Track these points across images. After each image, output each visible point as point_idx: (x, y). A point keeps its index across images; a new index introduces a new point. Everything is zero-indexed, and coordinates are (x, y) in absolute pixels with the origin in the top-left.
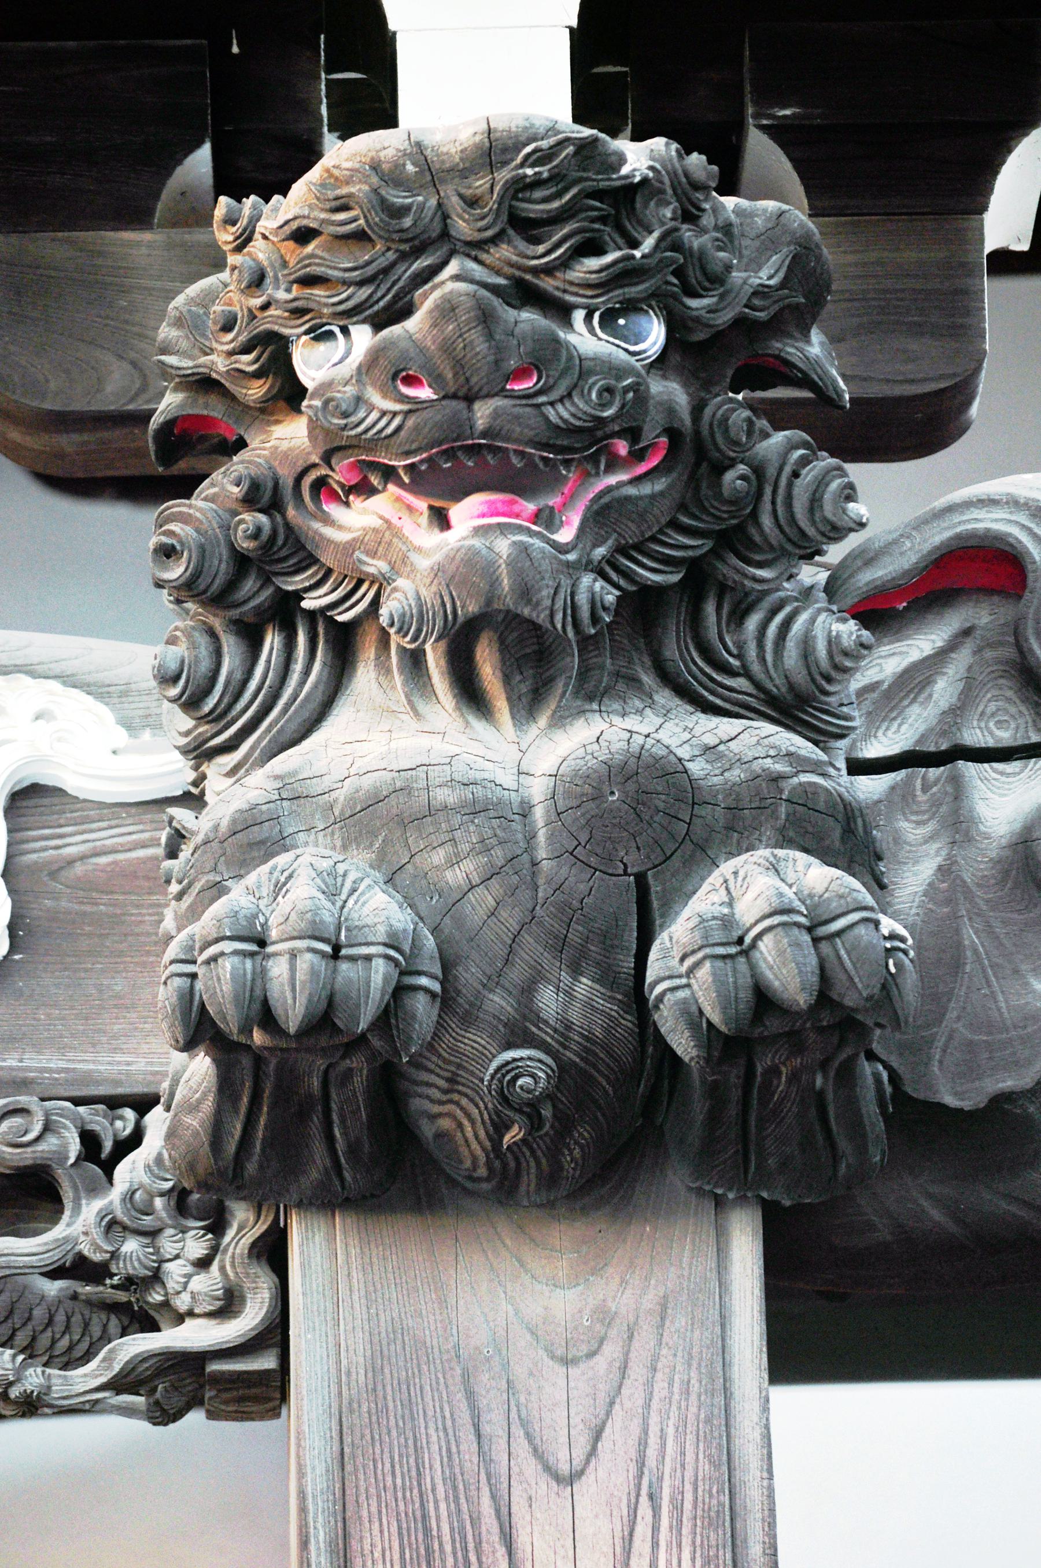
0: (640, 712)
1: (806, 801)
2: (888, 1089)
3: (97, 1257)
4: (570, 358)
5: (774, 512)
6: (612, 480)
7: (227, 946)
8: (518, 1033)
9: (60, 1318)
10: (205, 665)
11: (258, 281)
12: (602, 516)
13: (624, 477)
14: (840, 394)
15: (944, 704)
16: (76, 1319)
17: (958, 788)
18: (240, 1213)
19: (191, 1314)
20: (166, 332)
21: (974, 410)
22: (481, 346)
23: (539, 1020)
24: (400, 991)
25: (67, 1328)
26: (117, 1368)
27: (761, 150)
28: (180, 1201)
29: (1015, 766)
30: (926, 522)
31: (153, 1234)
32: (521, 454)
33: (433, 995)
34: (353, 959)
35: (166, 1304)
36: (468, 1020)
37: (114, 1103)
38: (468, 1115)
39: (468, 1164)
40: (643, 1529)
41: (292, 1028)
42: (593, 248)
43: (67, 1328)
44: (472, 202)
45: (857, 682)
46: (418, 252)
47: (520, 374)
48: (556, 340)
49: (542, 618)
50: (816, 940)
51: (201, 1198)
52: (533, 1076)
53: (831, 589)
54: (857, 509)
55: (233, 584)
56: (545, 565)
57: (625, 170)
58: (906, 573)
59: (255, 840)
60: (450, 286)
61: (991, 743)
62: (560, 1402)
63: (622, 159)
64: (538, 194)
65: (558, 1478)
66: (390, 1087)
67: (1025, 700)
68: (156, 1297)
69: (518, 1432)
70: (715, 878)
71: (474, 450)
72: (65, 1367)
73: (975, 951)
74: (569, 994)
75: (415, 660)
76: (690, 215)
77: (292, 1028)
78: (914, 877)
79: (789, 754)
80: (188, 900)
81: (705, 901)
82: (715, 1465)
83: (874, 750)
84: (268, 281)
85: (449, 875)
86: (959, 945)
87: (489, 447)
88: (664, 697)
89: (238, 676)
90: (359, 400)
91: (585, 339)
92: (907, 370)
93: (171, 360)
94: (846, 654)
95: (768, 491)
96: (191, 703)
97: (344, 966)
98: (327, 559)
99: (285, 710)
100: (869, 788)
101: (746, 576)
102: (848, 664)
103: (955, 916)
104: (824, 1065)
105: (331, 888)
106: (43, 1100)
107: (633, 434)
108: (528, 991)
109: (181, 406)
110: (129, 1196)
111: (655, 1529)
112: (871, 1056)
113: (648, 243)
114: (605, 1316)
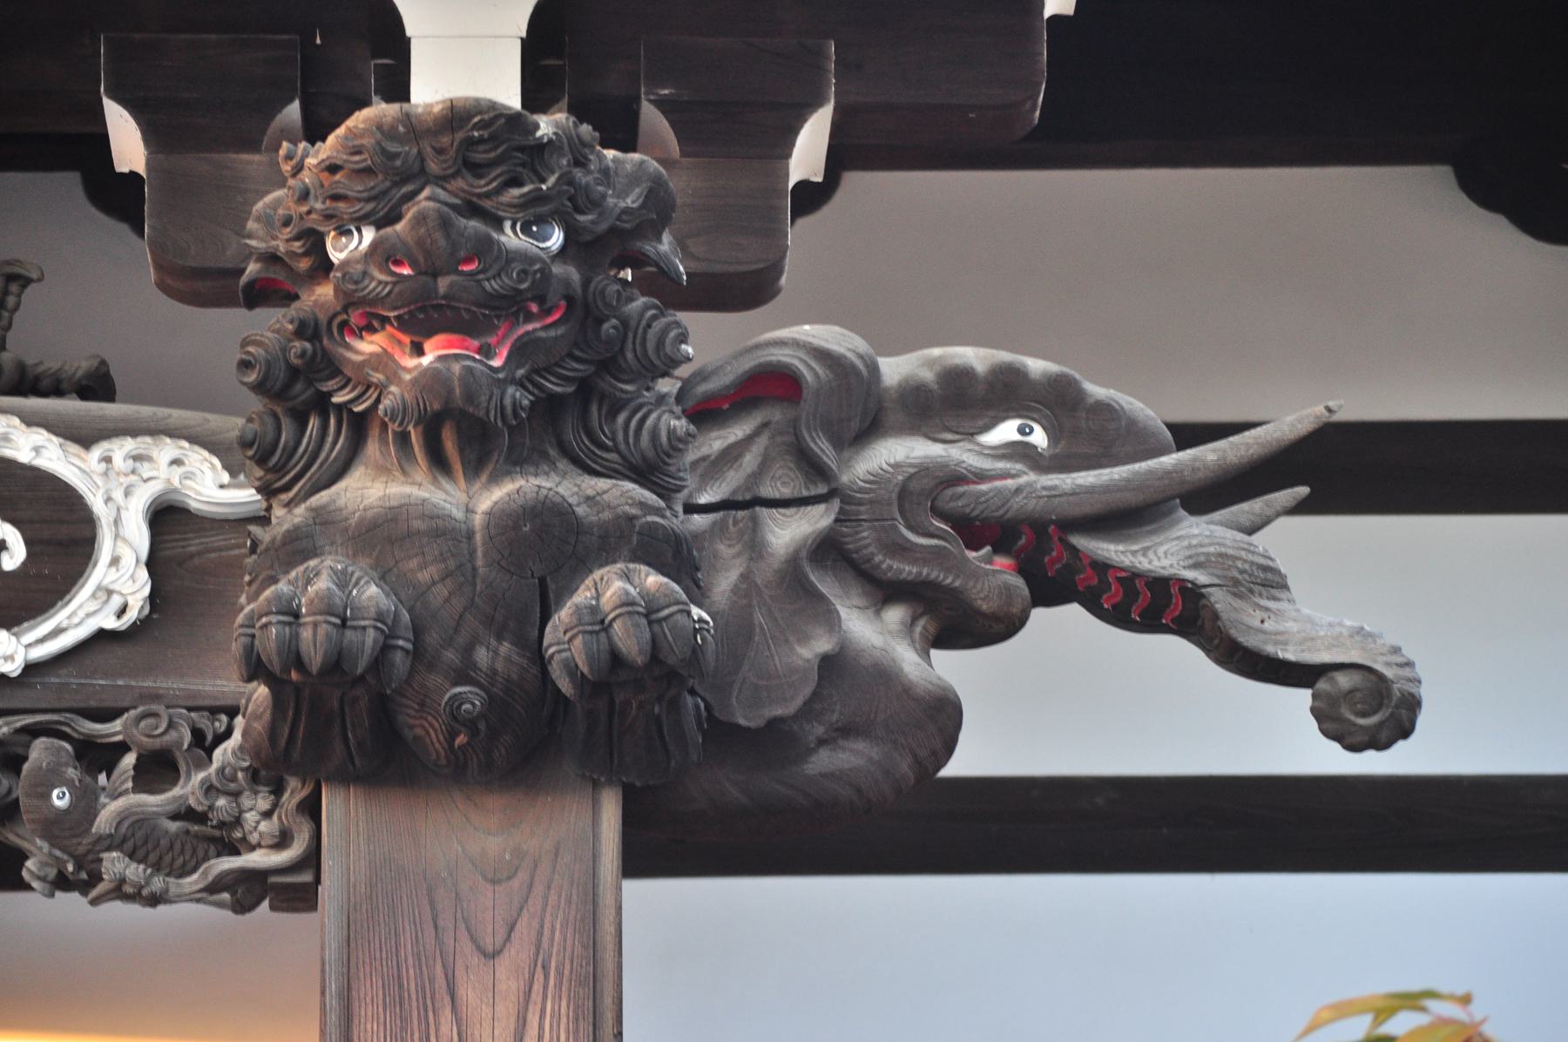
0: (547, 474)
1: (651, 531)
2: (704, 714)
3: (200, 809)
4: (500, 249)
5: (635, 350)
6: (530, 327)
7: (274, 618)
8: (461, 677)
9: (178, 846)
10: (270, 436)
11: (304, 196)
12: (521, 351)
13: (537, 325)
14: (679, 274)
15: (749, 470)
16: (188, 847)
17: (755, 521)
18: (293, 783)
19: (259, 846)
20: (251, 225)
21: (783, 280)
22: (442, 242)
23: (475, 667)
24: (385, 649)
25: (182, 852)
26: (210, 878)
27: (652, 117)
28: (254, 776)
29: (792, 511)
30: (741, 354)
31: (236, 795)
32: (469, 311)
33: (407, 652)
34: (354, 628)
35: (244, 839)
36: (431, 667)
37: (214, 711)
38: (432, 725)
39: (434, 756)
40: (538, 987)
41: (314, 670)
42: (517, 183)
43: (182, 852)
44: (440, 151)
45: (691, 456)
46: (405, 180)
47: (468, 261)
48: (490, 240)
49: (481, 414)
50: (650, 623)
51: (267, 771)
52: (473, 704)
53: (680, 397)
54: (688, 349)
55: (287, 386)
56: (484, 381)
57: (539, 133)
58: (727, 387)
59: (297, 548)
60: (425, 204)
61: (778, 496)
62: (489, 905)
63: (537, 127)
64: (481, 148)
65: (485, 955)
66: (384, 710)
67: (799, 468)
68: (238, 834)
69: (461, 926)
70: (589, 582)
71: (438, 307)
72: (181, 876)
73: (762, 629)
74: (496, 653)
75: (403, 439)
76: (580, 162)
77: (314, 670)
78: (724, 583)
79: (641, 503)
80: (254, 587)
81: (582, 596)
82: (585, 947)
83: (704, 499)
84: (312, 196)
85: (420, 576)
86: (751, 625)
87: (448, 306)
88: (563, 464)
89: (292, 443)
90: (365, 273)
91: (511, 239)
92: (739, 256)
93: (253, 243)
94: (680, 440)
95: (631, 335)
96: (261, 460)
97: (349, 633)
98: (348, 372)
99: (322, 465)
100: (699, 520)
101: (616, 388)
102: (681, 446)
103: (750, 606)
104: (659, 699)
105: (342, 580)
106: (168, 707)
107: (541, 299)
108: (468, 650)
109: (259, 272)
110: (221, 770)
111: (545, 988)
112: (692, 692)
113: (552, 180)
114: (519, 854)
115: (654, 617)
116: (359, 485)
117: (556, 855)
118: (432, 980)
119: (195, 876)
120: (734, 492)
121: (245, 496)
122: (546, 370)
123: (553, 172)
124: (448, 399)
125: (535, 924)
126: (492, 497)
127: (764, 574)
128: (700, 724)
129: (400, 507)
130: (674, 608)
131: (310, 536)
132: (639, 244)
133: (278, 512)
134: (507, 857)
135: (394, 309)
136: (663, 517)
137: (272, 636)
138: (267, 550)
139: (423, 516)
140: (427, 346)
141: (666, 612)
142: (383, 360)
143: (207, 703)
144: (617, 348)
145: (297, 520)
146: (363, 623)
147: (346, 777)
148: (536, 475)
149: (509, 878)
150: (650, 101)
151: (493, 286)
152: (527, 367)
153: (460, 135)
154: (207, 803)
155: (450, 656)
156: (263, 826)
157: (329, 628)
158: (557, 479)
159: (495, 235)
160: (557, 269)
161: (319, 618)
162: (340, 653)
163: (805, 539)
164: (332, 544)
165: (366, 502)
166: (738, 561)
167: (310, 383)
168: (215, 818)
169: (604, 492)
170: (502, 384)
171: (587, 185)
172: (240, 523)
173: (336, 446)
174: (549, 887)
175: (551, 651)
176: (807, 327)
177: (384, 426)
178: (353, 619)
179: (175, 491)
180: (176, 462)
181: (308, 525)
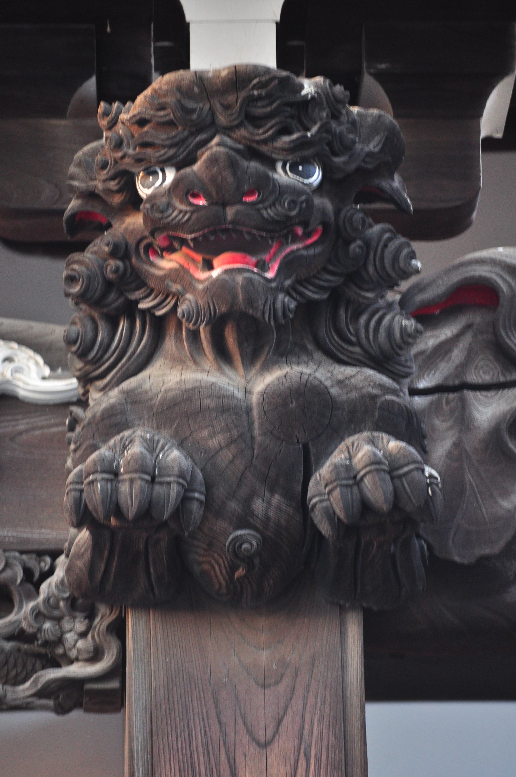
0: (307, 363)
1: (390, 406)
2: (427, 553)
3: (31, 630)
6: (295, 247)
7: (99, 476)
8: (244, 521)
9: (12, 660)
10: (90, 335)
12: (288, 265)
13: (300, 245)
14: (409, 207)
16: (19, 661)
17: (464, 404)
18: (103, 610)
19: (77, 659)
20: (73, 169)
21: (474, 215)
22: (230, 179)
23: (252, 514)
24: (185, 500)
25: (15, 666)
26: (39, 686)
28: (72, 604)
31: (58, 620)
32: (249, 233)
33: (201, 502)
34: (161, 483)
35: (65, 655)
37: (40, 554)
39: (217, 586)
41: (131, 516)
42: (286, 131)
43: (15, 666)
45: (414, 351)
46: (199, 131)
47: (250, 193)
49: (259, 315)
50: (392, 478)
52: (251, 545)
53: (402, 303)
55: (104, 295)
56: (261, 289)
57: (304, 92)
58: (440, 297)
59: (113, 423)
61: (480, 381)
62: (261, 705)
63: (302, 87)
64: (260, 104)
65: (259, 744)
66: (178, 547)
68: (60, 651)
69: (240, 722)
70: (342, 446)
71: (226, 231)
74: (269, 503)
75: (194, 336)
76: (335, 115)
77: (131, 516)
78: (441, 449)
80: (79, 453)
81: (338, 457)
83: (422, 384)
85: (210, 443)
88: (318, 356)
89: (106, 341)
91: (282, 176)
93: (76, 183)
94: (409, 335)
96: (82, 355)
97: (157, 488)
98: (152, 283)
100: (419, 402)
101: (360, 296)
102: (410, 340)
105: (151, 446)
107: (305, 224)
108: (248, 502)
110: (47, 600)
112: (418, 536)
113: (315, 129)
114: (283, 664)
115: (396, 473)
116: (160, 372)
117: (313, 665)
118: (218, 765)
119: (27, 684)
120: (446, 379)
121: (67, 385)
122: (315, 277)
123: (315, 123)
124: (233, 304)
125: (298, 719)
126: (266, 381)
127: (472, 443)
128: (424, 561)
129: (194, 389)
130: (411, 467)
131: (123, 413)
132: (377, 181)
133: (94, 396)
134: (274, 666)
135: (192, 232)
136: (398, 396)
137: (97, 491)
138: (89, 424)
139: (211, 396)
140: (216, 262)
141: (405, 469)
142: (180, 274)
143: (35, 547)
144: (362, 263)
145: (112, 401)
146: (168, 479)
147: (146, 605)
148: (298, 364)
149: (277, 683)
150: (371, 74)
151: (269, 213)
152: (293, 278)
153: (243, 94)
154: (36, 625)
155: (233, 506)
156: (81, 644)
157: (143, 483)
158: (315, 367)
159: (270, 174)
160: (318, 201)
161: (136, 475)
162: (150, 503)
163: (505, 415)
164: (140, 419)
165: (166, 386)
166: (451, 433)
167: (121, 293)
168: (41, 638)
169: (352, 377)
170: (275, 291)
171: (341, 134)
172: (61, 406)
173: (141, 343)
174: (308, 691)
175: (314, 501)
176: (501, 249)
177: (179, 324)
178: (160, 476)
179: (8, 382)
180: (8, 359)
181: (120, 404)
